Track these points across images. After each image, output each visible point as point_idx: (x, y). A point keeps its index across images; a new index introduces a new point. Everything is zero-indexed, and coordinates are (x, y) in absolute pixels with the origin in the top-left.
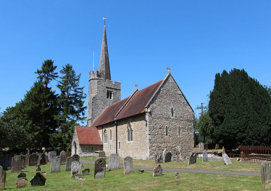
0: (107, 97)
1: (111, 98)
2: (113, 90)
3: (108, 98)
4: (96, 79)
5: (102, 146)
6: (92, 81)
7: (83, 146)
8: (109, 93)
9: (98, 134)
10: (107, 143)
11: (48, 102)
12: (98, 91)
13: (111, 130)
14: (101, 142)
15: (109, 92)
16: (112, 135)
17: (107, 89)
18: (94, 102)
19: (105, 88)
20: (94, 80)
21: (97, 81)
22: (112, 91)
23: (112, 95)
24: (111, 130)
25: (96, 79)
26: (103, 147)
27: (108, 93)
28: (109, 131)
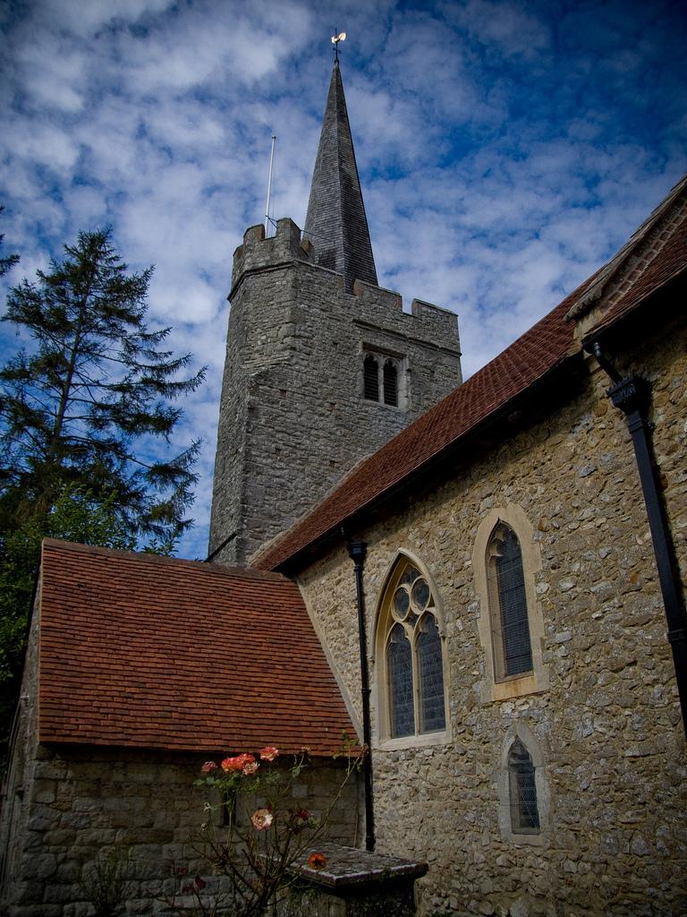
0: (370, 345)
1: (392, 399)
2: (413, 351)
3: (370, 393)
4: (280, 266)
5: (365, 770)
6: (251, 282)
7: (94, 771)
8: (376, 365)
9: (303, 636)
10: (443, 737)
11: (396, 907)
12: (299, 343)
13: (504, 539)
14: (350, 735)
15: (382, 361)
16: (535, 589)
17: (361, 338)
18: (264, 408)
19: (348, 325)
20: (266, 278)
21: (290, 276)
22: (402, 357)
23: (403, 381)
24: (504, 539)
25: (280, 266)
26: (377, 784)
27: (370, 366)
28: (477, 557)
